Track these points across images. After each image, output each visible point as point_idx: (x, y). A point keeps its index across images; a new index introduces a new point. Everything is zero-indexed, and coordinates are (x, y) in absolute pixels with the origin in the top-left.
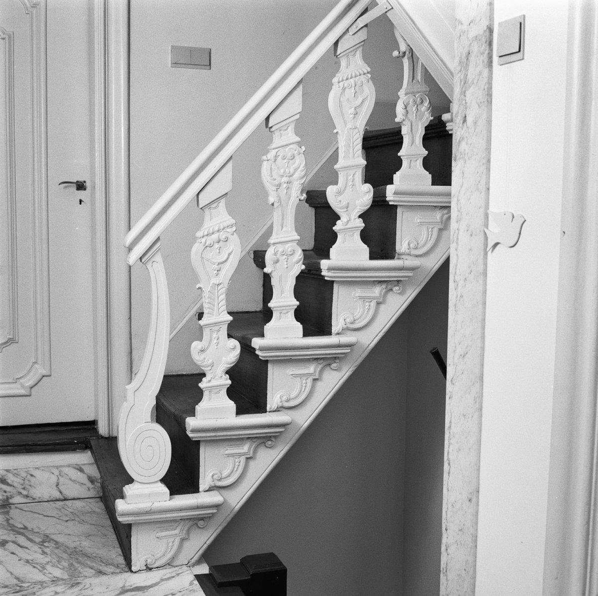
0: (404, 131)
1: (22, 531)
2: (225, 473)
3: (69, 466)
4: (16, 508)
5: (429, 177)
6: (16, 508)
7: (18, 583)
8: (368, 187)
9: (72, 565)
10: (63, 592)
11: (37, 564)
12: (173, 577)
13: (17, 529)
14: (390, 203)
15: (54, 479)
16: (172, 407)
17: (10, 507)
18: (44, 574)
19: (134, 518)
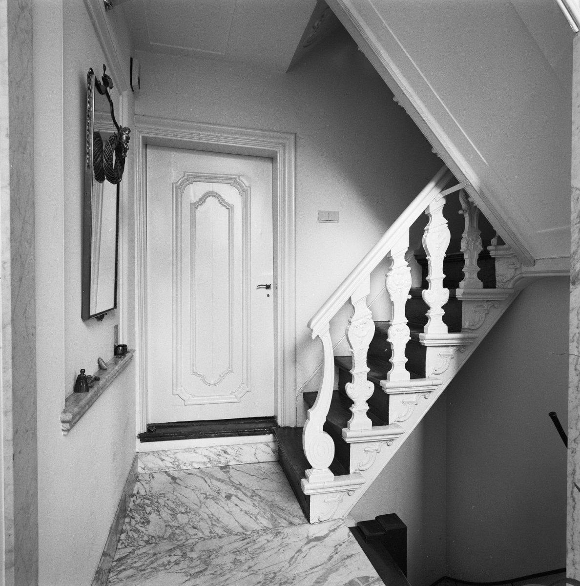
0: (466, 256)
1: (238, 486)
2: (365, 462)
3: (261, 443)
4: (233, 468)
5: (481, 283)
6: (233, 468)
7: (244, 531)
8: (447, 291)
9: (272, 516)
10: (272, 541)
11: (252, 514)
12: (336, 529)
13: (236, 485)
14: (459, 299)
15: (253, 451)
16: (336, 422)
17: (229, 467)
18: (258, 524)
19: (313, 492)
